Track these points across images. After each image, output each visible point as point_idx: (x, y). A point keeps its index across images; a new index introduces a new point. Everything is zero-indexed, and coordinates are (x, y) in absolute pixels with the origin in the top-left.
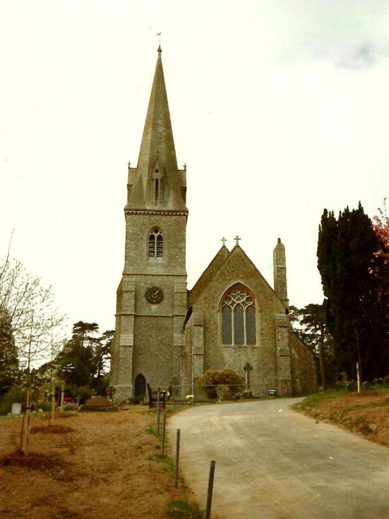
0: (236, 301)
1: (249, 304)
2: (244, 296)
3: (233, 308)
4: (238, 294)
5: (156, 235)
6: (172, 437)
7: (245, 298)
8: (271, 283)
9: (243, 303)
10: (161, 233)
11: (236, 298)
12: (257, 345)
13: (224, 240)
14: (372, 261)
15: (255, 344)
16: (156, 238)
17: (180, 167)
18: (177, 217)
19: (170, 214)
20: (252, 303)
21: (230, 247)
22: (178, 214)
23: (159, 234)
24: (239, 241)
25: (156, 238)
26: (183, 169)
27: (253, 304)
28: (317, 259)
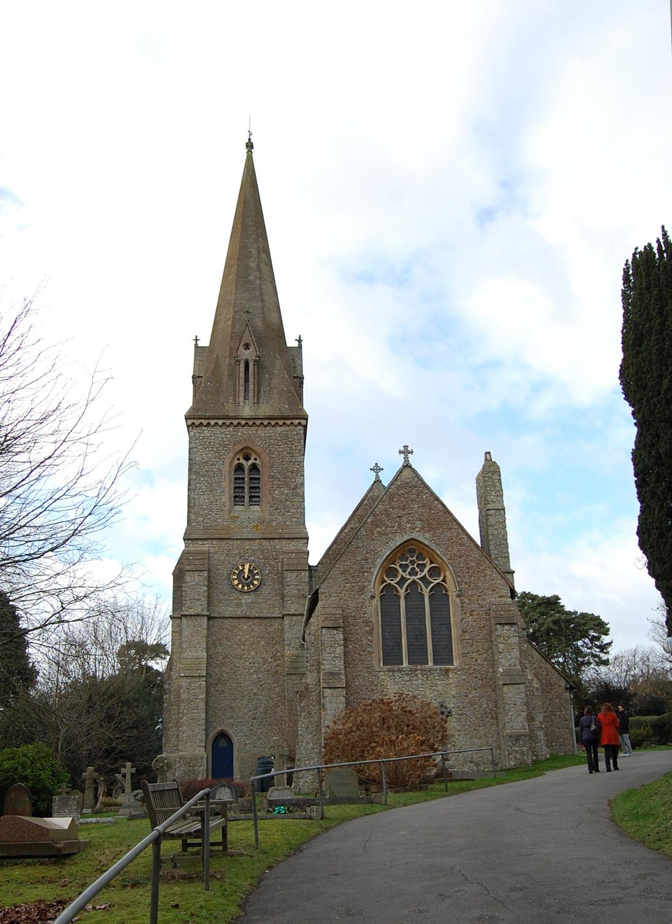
0: (408, 577)
2: (424, 566)
4: (412, 562)
5: (247, 465)
7: (426, 570)
9: (423, 579)
10: (255, 459)
11: (409, 570)
13: (377, 469)
16: (246, 471)
17: (291, 342)
18: (286, 428)
19: (273, 422)
20: (442, 578)
22: (288, 422)
23: (251, 461)
24: (410, 455)
25: (246, 471)
26: (296, 344)
27: (444, 580)
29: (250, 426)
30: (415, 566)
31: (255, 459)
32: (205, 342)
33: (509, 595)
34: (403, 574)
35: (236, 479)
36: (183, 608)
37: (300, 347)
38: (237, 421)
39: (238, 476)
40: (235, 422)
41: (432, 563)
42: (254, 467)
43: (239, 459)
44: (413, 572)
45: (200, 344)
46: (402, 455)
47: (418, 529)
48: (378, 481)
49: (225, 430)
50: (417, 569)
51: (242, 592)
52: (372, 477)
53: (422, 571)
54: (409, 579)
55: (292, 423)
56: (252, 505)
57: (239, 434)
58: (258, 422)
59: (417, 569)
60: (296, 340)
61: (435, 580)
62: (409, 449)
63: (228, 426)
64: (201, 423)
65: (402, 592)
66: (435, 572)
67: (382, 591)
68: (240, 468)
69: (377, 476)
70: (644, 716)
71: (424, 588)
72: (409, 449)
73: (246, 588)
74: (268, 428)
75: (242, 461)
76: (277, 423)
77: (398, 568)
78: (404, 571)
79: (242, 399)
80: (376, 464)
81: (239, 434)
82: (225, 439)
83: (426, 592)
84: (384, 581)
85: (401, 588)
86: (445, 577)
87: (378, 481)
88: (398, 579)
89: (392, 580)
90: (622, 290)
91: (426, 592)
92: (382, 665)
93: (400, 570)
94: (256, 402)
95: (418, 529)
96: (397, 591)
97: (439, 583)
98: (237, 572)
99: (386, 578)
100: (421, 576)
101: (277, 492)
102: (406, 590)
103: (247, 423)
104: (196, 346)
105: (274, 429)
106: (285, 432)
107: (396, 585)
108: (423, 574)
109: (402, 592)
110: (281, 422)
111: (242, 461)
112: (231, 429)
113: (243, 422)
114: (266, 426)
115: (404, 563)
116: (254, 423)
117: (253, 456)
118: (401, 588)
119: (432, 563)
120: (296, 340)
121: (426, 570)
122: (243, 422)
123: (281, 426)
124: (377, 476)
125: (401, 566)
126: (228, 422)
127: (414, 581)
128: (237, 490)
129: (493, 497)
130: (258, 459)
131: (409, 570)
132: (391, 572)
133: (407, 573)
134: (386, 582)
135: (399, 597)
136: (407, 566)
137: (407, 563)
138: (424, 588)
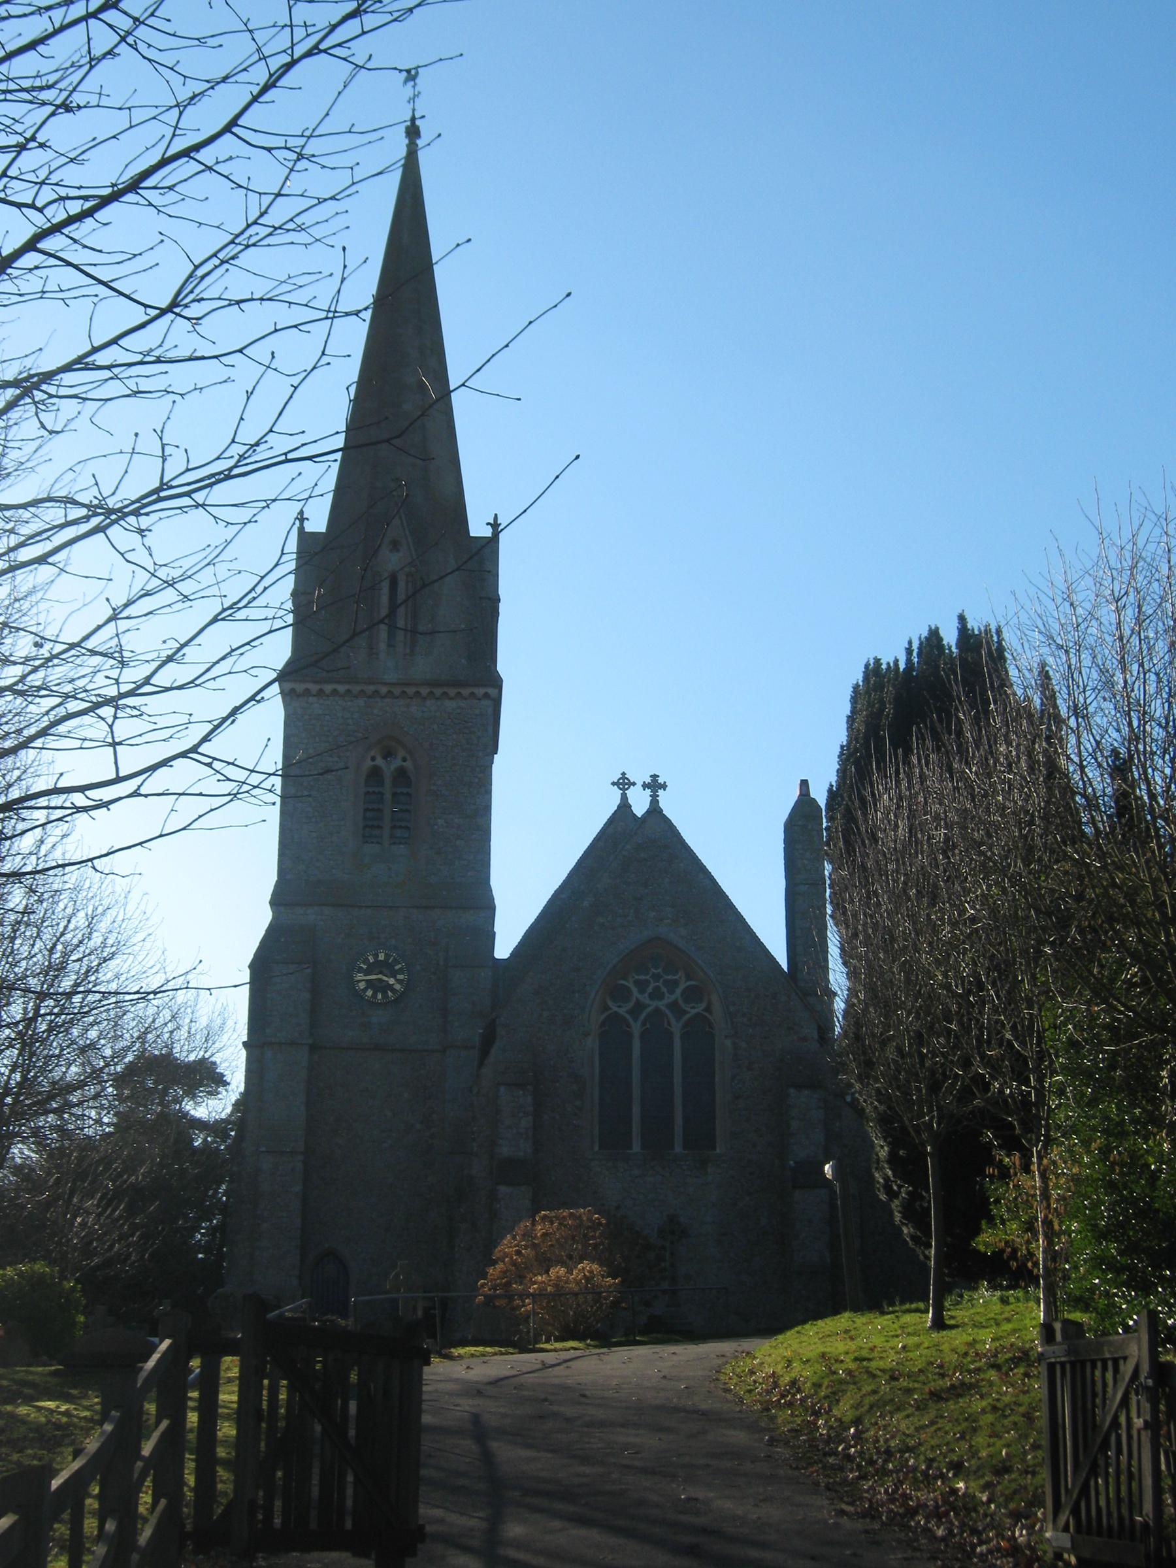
0: (648, 1001)
1: (696, 1011)
2: (675, 983)
3: (639, 1023)
4: (657, 977)
5: (389, 768)
6: (224, 1439)
7: (679, 991)
8: (778, 949)
9: (674, 1006)
10: (404, 760)
11: (650, 990)
12: (718, 1151)
13: (624, 783)
14: (200, 1256)
15: (714, 1148)
16: (388, 782)
17: (478, 528)
18: (462, 703)
19: (438, 692)
20: (703, 1006)
21: (640, 803)
22: (466, 692)
23: (397, 763)
24: (661, 792)
25: (388, 782)
26: (487, 532)
27: (708, 1009)
28: (495, 930)
29: (397, 698)
30: (660, 984)
31: (404, 760)
32: (318, 522)
33: (816, 1036)
34: (640, 997)
35: (368, 793)
36: (267, 1031)
37: (494, 540)
38: (372, 688)
39: (371, 790)
40: (370, 689)
41: (689, 978)
42: (401, 773)
43: (373, 759)
44: (657, 995)
45: (309, 527)
46: (648, 792)
47: (669, 921)
48: (624, 806)
49: (349, 703)
50: (664, 990)
51: (372, 1004)
52: (614, 798)
53: (672, 992)
54: (649, 1005)
55: (473, 694)
56: (394, 843)
57: (376, 711)
58: (411, 691)
59: (664, 990)
60: (488, 524)
61: (693, 1008)
62: (661, 780)
63: (356, 697)
64: (307, 690)
65: (636, 1028)
66: (694, 994)
67: (603, 1024)
68: (375, 774)
69: (624, 797)
70: (773, 1327)
71: (673, 1021)
72: (661, 780)
73: (380, 996)
74: (428, 703)
75: (379, 761)
76: (445, 693)
77: (631, 985)
78: (642, 991)
79: (383, 646)
80: (624, 774)
81: (376, 711)
82: (350, 721)
83: (676, 1029)
84: (606, 1008)
85: (636, 1019)
86: (710, 1003)
87: (624, 806)
88: (631, 1005)
89: (620, 1007)
90: (934, 635)
91: (676, 1029)
92: (596, 1149)
93: (635, 990)
94: (408, 651)
95: (669, 921)
96: (628, 1026)
97: (698, 1014)
98: (365, 967)
99: (610, 1003)
100: (670, 1000)
101: (440, 822)
102: (644, 1024)
103: (390, 692)
104: (301, 530)
105: (439, 703)
106: (459, 711)
107: (627, 1016)
108: (673, 997)
109: (636, 1028)
110: (452, 692)
111: (379, 761)
112: (361, 702)
113: (384, 690)
114: (425, 699)
115: (642, 977)
116: (404, 692)
117: (401, 753)
118: (636, 1019)
119: (689, 978)
120: (488, 524)
121: (679, 991)
122: (384, 690)
123: (451, 699)
124: (624, 797)
125: (637, 983)
126: (356, 689)
127: (657, 1011)
128: (369, 814)
129: (806, 862)
130: (408, 758)
131: (650, 990)
132: (620, 994)
133: (646, 995)
134: (610, 1009)
135: (630, 1036)
136: (647, 982)
137: (648, 977)
138: (673, 1021)
